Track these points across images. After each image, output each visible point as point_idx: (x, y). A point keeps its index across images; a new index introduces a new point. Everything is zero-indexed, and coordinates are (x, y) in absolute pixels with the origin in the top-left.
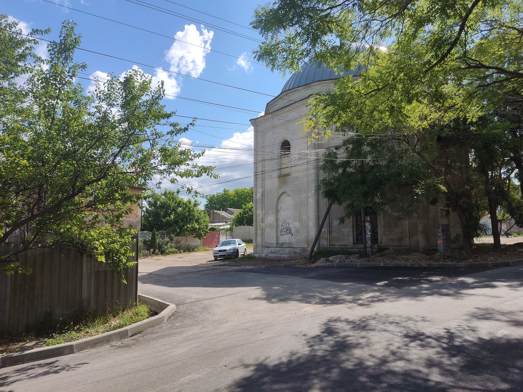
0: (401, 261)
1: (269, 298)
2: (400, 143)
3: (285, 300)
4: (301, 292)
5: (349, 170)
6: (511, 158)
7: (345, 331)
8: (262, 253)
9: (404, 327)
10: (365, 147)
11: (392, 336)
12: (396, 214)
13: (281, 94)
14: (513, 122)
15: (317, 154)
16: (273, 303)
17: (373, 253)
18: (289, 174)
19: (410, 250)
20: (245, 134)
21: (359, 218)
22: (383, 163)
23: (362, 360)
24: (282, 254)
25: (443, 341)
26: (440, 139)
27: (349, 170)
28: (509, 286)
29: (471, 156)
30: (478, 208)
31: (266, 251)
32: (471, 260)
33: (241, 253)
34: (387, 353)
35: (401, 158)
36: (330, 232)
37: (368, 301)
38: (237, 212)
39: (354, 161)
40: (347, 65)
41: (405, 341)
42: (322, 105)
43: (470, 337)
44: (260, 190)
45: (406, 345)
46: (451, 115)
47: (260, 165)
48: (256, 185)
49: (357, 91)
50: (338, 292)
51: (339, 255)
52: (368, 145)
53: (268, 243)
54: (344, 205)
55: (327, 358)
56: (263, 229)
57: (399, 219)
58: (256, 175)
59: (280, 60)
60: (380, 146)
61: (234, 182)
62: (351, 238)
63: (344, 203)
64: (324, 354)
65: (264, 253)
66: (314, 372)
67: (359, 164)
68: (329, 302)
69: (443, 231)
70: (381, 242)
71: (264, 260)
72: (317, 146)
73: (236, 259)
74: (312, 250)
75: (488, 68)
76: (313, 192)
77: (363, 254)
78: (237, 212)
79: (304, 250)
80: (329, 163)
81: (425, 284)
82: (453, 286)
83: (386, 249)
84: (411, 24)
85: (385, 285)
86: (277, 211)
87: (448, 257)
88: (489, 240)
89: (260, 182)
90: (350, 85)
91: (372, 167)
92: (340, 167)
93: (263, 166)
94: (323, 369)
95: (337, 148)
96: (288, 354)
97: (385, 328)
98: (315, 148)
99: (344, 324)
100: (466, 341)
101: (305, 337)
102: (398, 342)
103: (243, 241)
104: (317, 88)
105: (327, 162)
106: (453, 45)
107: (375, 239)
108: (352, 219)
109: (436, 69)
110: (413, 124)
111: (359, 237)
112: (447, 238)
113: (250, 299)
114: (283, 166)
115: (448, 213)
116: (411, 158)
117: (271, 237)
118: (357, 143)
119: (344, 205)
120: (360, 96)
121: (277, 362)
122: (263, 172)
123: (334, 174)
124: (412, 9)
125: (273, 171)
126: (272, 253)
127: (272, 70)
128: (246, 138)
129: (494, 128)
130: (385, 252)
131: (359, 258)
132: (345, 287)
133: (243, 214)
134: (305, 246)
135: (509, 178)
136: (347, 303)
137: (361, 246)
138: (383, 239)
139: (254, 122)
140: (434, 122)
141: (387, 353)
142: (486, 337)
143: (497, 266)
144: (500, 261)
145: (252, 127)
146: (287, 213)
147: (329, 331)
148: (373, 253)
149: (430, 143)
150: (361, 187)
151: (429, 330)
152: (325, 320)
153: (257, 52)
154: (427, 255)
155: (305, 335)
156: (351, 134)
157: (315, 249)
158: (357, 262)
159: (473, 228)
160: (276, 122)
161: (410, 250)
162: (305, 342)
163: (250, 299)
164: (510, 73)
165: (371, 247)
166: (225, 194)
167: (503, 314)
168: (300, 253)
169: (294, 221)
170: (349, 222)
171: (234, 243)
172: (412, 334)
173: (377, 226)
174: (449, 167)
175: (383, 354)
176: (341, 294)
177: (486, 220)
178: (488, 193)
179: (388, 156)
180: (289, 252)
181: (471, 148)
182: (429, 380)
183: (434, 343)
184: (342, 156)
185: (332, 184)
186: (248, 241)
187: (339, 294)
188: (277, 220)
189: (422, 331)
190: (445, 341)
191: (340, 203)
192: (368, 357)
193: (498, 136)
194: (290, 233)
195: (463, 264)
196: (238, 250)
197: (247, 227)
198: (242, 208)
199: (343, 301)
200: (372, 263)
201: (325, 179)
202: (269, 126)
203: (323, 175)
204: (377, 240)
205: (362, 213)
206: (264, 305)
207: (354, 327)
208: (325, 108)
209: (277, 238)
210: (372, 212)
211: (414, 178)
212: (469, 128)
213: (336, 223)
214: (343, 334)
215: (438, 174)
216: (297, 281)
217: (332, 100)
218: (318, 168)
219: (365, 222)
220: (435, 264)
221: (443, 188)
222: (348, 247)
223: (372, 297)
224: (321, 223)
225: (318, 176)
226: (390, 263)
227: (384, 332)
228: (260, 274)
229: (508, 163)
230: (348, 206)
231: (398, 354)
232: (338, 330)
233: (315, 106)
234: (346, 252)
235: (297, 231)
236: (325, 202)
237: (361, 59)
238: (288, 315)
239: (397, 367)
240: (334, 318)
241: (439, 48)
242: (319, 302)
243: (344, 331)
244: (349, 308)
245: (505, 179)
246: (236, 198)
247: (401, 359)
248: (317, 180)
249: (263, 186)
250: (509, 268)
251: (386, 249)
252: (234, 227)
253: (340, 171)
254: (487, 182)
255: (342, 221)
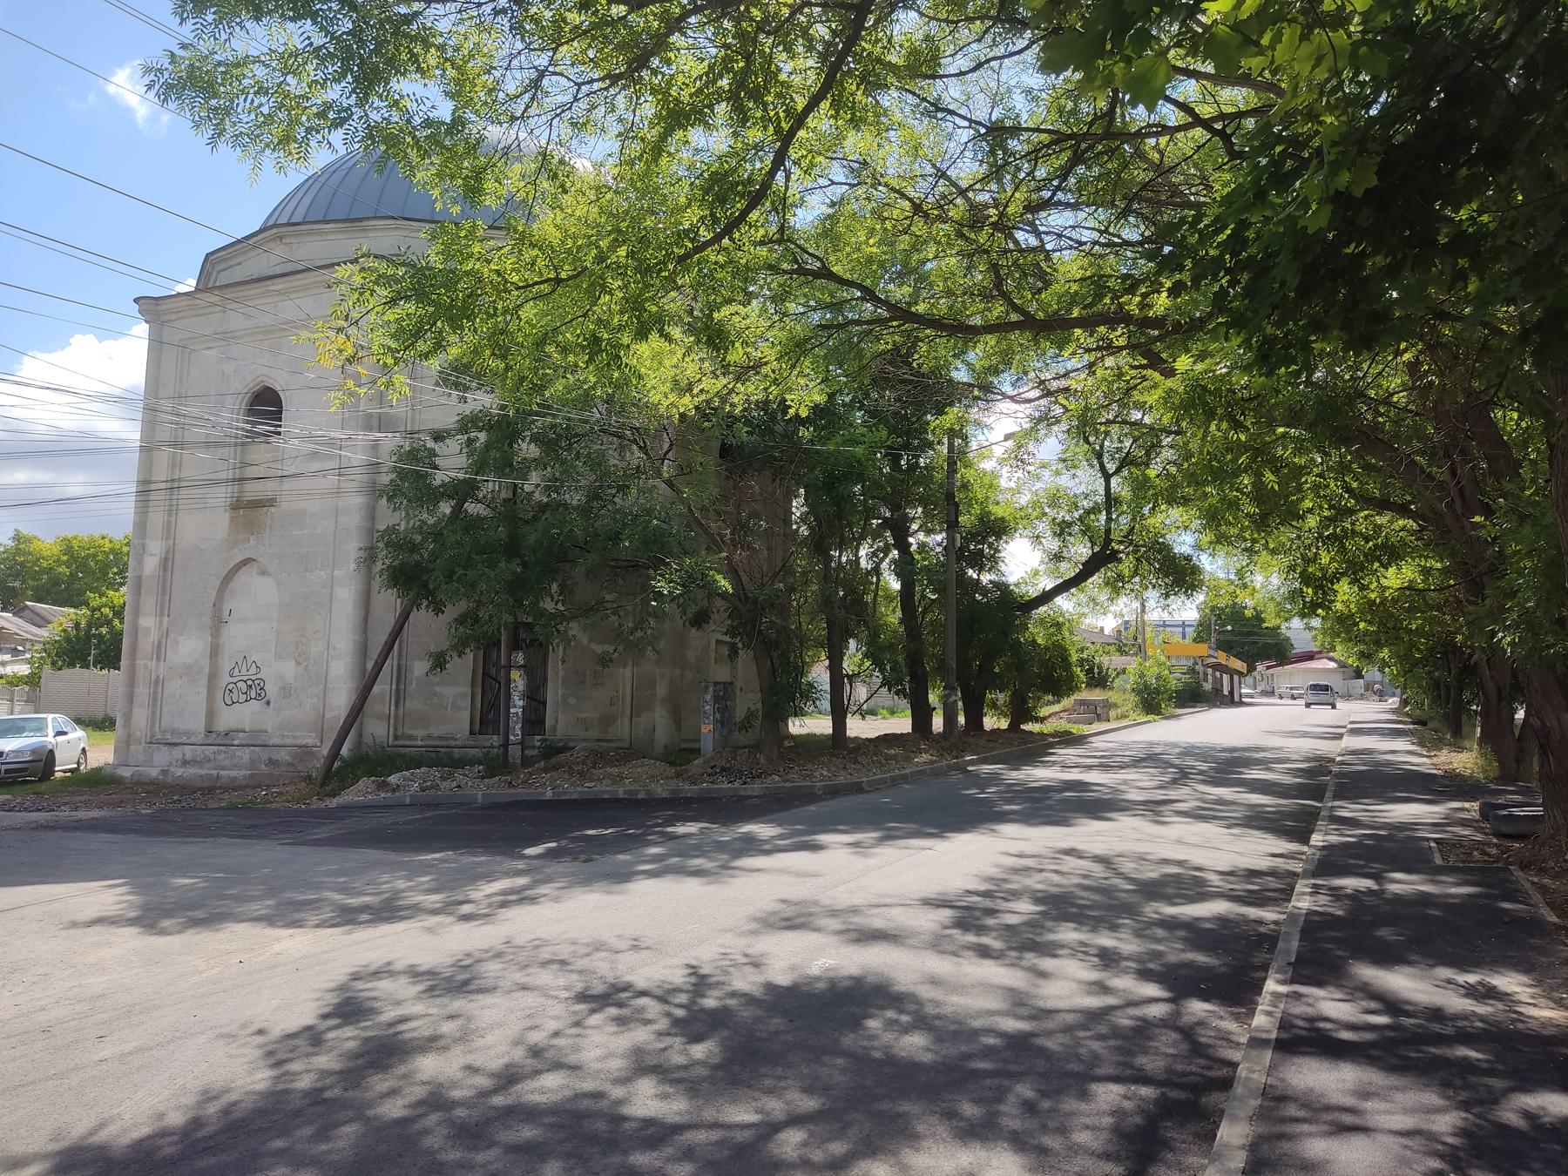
0: (601, 785)
1: (148, 919)
2: (622, 447)
3: (212, 920)
4: (272, 892)
5: (471, 508)
6: (885, 519)
7: (400, 1002)
8: (149, 763)
9: (580, 972)
10: (524, 446)
11: (541, 1000)
12: (598, 649)
13: (261, 231)
14: (893, 431)
15: (375, 447)
16: (163, 932)
17: (526, 762)
18: (271, 502)
19: (630, 753)
20: (124, 342)
21: (494, 658)
22: (575, 499)
23: (440, 1085)
24: (223, 768)
25: (677, 1001)
26: (725, 451)
27: (471, 508)
28: (856, 845)
29: (798, 507)
30: (803, 640)
31: (162, 757)
32: (777, 778)
33: (64, 764)
34: (518, 1054)
35: (623, 489)
36: (399, 697)
37: (490, 905)
38: (63, 618)
39: (491, 485)
40: (473, 191)
41: (575, 1013)
42: (383, 292)
43: (746, 982)
44: (155, 547)
45: (577, 1024)
46: (752, 390)
47: (163, 457)
48: (141, 526)
49: (498, 272)
50: (401, 884)
51: (423, 769)
52: (535, 439)
53: (174, 732)
54: (451, 612)
55: (328, 1094)
56: (157, 683)
57: (604, 661)
58: (145, 490)
59: (245, 118)
60: (569, 449)
61: (53, 508)
62: (465, 715)
63: (449, 606)
64: (319, 1085)
65: (158, 764)
66: (278, 1144)
67: (503, 495)
68: (365, 917)
69: (716, 699)
70: (554, 729)
71: (154, 789)
72: (375, 422)
73: (43, 787)
74: (335, 753)
75: (850, 284)
76: (353, 566)
77: (496, 766)
78: (63, 618)
79: (306, 752)
80: (411, 478)
81: (656, 844)
82: (721, 847)
83: (564, 749)
84: (658, 116)
85: (551, 855)
86: (218, 623)
87: (723, 769)
88: (821, 725)
89: (157, 518)
90: (477, 248)
91: (543, 508)
92: (443, 495)
93: (175, 464)
94: (307, 1131)
95: (438, 436)
96: (189, 1100)
97: (524, 980)
98: (368, 428)
99: (404, 980)
100: (733, 994)
101: (260, 1039)
102: (557, 1018)
103: (79, 721)
104: (385, 239)
105: (402, 474)
106: (755, 200)
107: (535, 719)
108: (471, 656)
109: (711, 254)
110: (654, 397)
111: (489, 715)
112: (724, 720)
113: (74, 925)
114: (251, 472)
115: (734, 652)
116: (653, 494)
117: (187, 710)
118: (504, 430)
119: (451, 612)
120: (503, 287)
121: (145, 1131)
122: (174, 485)
123: (425, 516)
124: (664, 75)
125: (215, 483)
126: (185, 763)
127: (213, 142)
128: (124, 359)
129: (853, 442)
130: (562, 757)
131: (483, 778)
132: (424, 868)
133: (89, 626)
134: (309, 741)
135: (877, 571)
136: (425, 917)
137: (495, 740)
138: (559, 720)
139: (151, 308)
140: (708, 402)
141: (518, 1054)
142: (783, 980)
143: (833, 792)
144: (841, 779)
145: (142, 329)
146: (257, 624)
147: (349, 1008)
148: (526, 762)
149: (700, 459)
150: (502, 565)
151: (644, 972)
152: (337, 973)
153: (160, 71)
154: (672, 764)
155: (260, 1032)
156: (483, 400)
157: (344, 751)
158: (477, 788)
159: (787, 694)
160: (236, 321)
161: (630, 753)
162: (258, 1053)
163: (74, 925)
164: (892, 307)
165: (522, 743)
166: (18, 552)
167: (833, 913)
168: (290, 764)
169: (278, 657)
170: (464, 666)
171: (40, 728)
172: (599, 988)
173: (546, 680)
174: (740, 527)
175: (506, 1060)
176: (411, 889)
177: (819, 674)
178: (826, 603)
179: (587, 479)
180: (252, 761)
181: (798, 485)
182: (624, 1118)
183: (652, 1007)
184: (452, 462)
185: (414, 548)
186: (98, 724)
187: (403, 891)
188: (215, 652)
189: (627, 978)
190: (682, 998)
191: (438, 611)
192: (460, 1075)
193: (859, 462)
194: (258, 697)
195: (755, 788)
196: (51, 752)
197: (97, 674)
198: (86, 604)
199: (415, 911)
200: (521, 792)
201: (392, 530)
202: (209, 331)
203: (389, 517)
204: (543, 722)
205: (504, 641)
206: (130, 940)
207: (431, 989)
208: (392, 302)
209: (211, 714)
210: (532, 641)
211: (655, 552)
212: (796, 432)
213: (420, 668)
214: (390, 1014)
215: (714, 544)
216: (265, 856)
217: (420, 284)
218: (374, 492)
219: (509, 667)
220: (688, 789)
221: (724, 584)
222: (452, 743)
223: (504, 893)
224: (370, 666)
225: (372, 517)
226: (572, 789)
227: (521, 993)
228: (132, 837)
229: (877, 535)
230: (461, 620)
231: (549, 1055)
232: (376, 1005)
233: (361, 290)
234: (443, 758)
235: (286, 691)
236: (388, 603)
237: (513, 180)
238: (215, 971)
239: (542, 1091)
240: (373, 968)
241: (722, 200)
242: (333, 918)
243: (398, 1003)
244: (429, 930)
245: (868, 573)
246: (63, 569)
247: (557, 1066)
248: (371, 530)
249: (169, 532)
250: (859, 799)
251: (564, 749)
252: (47, 669)
253: (446, 508)
254: (826, 576)
255: (439, 662)
